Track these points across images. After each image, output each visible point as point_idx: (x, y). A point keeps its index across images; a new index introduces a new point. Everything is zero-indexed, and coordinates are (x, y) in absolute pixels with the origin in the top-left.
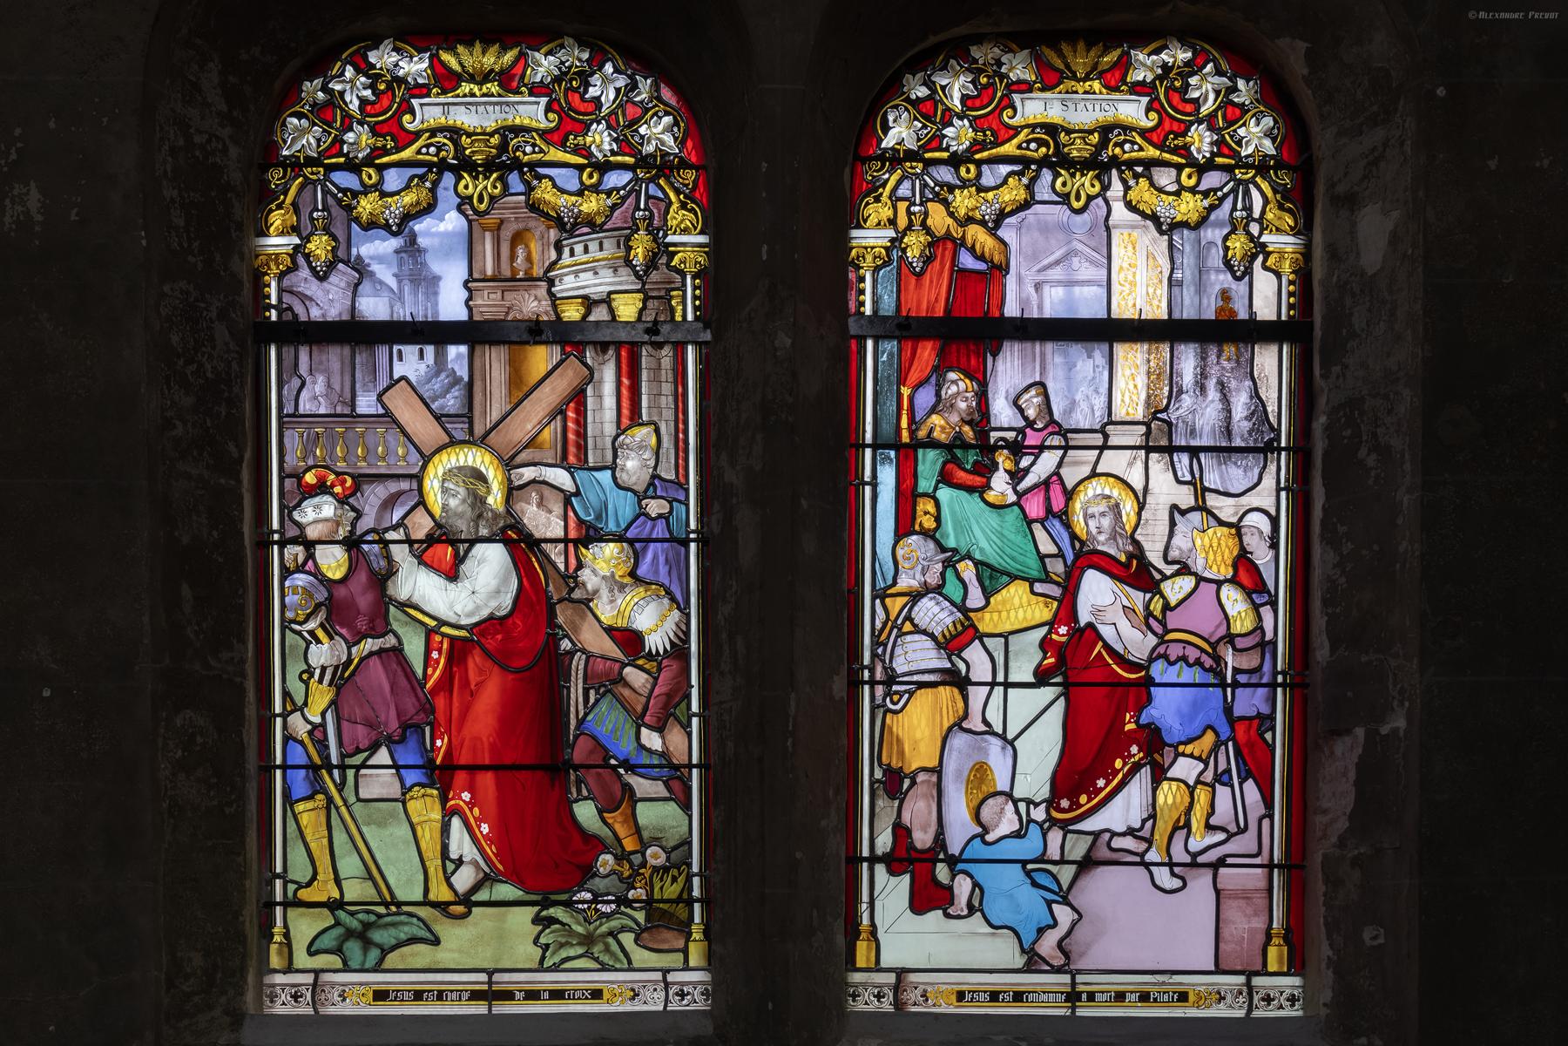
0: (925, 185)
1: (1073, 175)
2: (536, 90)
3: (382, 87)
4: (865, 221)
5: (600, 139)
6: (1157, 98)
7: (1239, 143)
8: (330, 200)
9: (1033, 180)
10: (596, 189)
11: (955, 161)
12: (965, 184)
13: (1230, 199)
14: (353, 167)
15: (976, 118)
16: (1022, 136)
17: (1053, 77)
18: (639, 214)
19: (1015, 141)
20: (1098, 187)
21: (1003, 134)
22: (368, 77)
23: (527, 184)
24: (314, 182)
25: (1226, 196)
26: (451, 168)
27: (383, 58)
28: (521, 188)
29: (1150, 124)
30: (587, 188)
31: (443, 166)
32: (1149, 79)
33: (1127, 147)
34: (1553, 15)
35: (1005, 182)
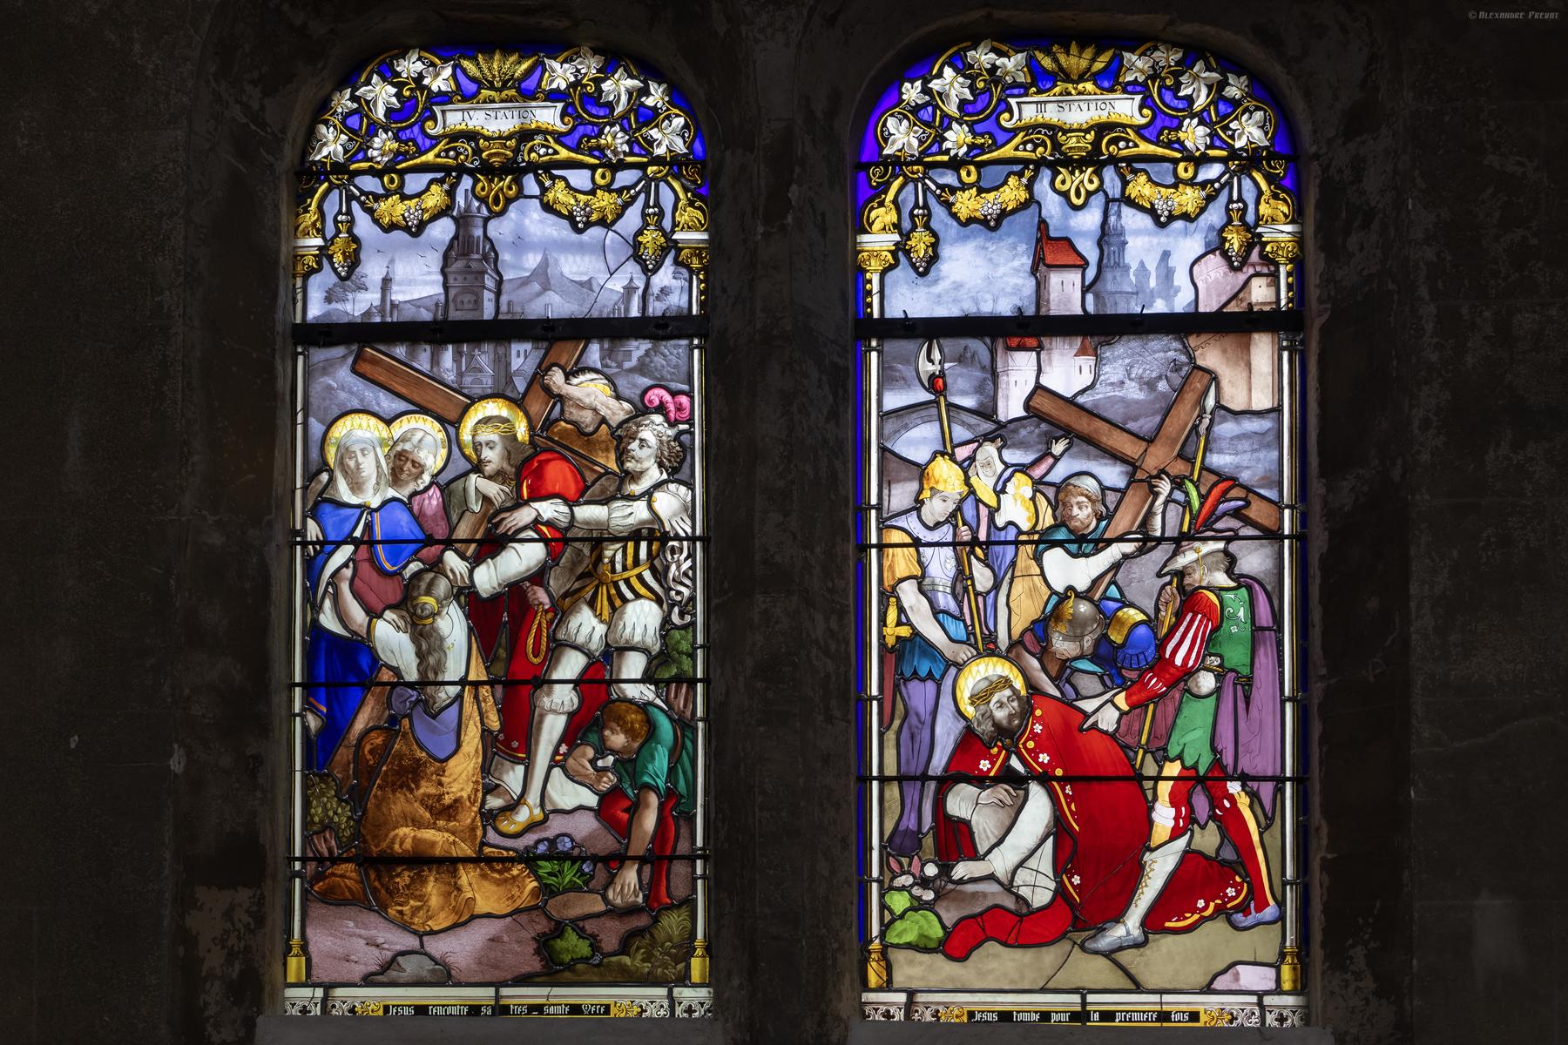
0: (926, 189)
1: (1072, 173)
2: (554, 96)
4: (870, 225)
5: (1194, 135)
6: (573, 104)
7: (1232, 137)
9: (1032, 181)
10: (1191, 183)
11: (955, 164)
13: (643, 196)
14: (955, 164)
15: (400, 129)
16: (1018, 140)
19: (436, 150)
21: (1001, 137)
22: (393, 85)
23: (540, 184)
24: (915, 181)
25: (1223, 186)
26: (471, 172)
27: (983, 57)
28: (536, 191)
29: (1144, 121)
30: (600, 187)
31: (462, 170)
32: (1141, 79)
33: (1122, 144)
34: (1552, 16)
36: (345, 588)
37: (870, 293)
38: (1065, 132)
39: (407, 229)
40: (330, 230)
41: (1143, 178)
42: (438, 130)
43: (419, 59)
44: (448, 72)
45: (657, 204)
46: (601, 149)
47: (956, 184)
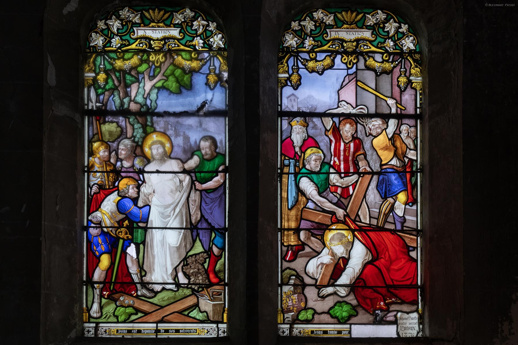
1: (348, 57)
3: (124, 23)
7: (402, 45)
8: (106, 62)
9: (334, 58)
10: (196, 59)
12: (311, 59)
13: (209, 62)
16: (137, 42)
17: (147, 22)
18: (102, 66)
20: (164, 59)
21: (132, 41)
25: (207, 61)
31: (337, 53)
34: (513, 5)
35: (325, 58)
36: (205, 186)
37: (421, 94)
38: (346, 42)
39: (318, 72)
40: (291, 72)
41: (371, 59)
42: (328, 38)
43: (322, 13)
44: (332, 18)
45: (214, 65)
46: (384, 47)
47: (308, 58)
